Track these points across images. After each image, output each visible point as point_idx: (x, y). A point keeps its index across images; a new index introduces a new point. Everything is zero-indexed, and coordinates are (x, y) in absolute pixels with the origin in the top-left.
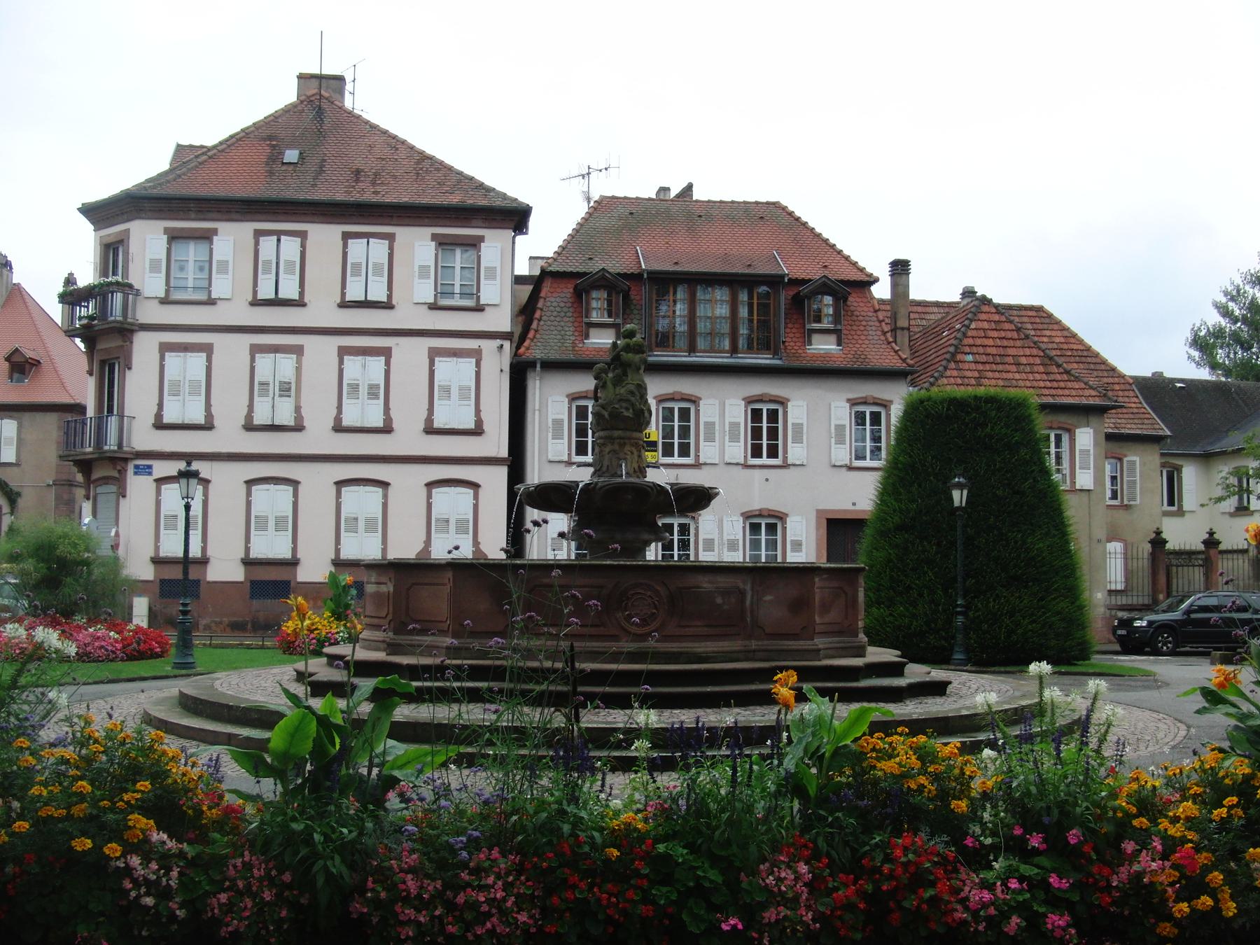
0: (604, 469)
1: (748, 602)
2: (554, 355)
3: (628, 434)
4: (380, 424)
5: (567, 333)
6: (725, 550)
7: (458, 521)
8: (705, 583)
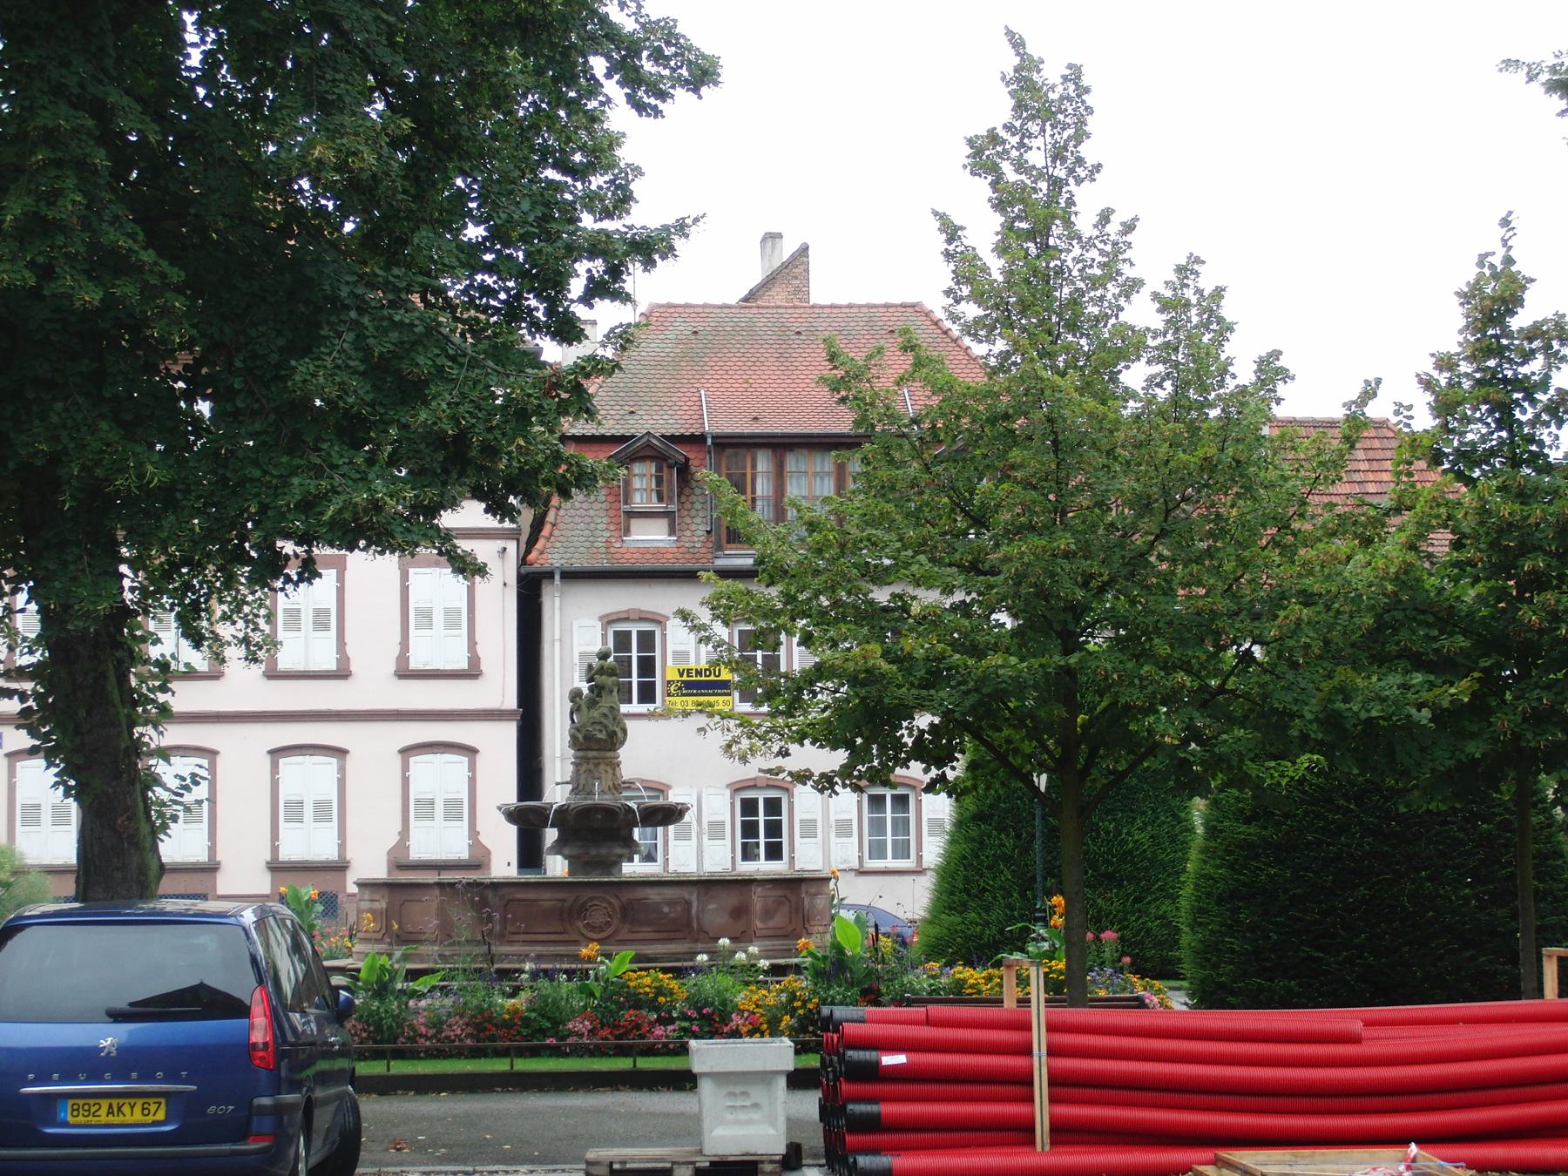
0: (581, 787)
1: (694, 911)
2: (580, 562)
3: (602, 754)
4: (331, 665)
5: (599, 527)
6: (833, 835)
7: (447, 802)
8: (653, 895)
